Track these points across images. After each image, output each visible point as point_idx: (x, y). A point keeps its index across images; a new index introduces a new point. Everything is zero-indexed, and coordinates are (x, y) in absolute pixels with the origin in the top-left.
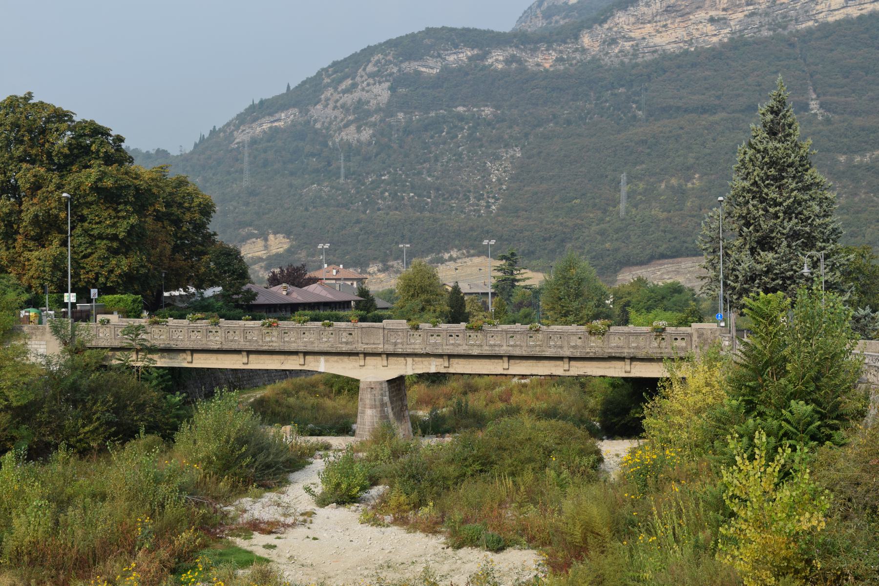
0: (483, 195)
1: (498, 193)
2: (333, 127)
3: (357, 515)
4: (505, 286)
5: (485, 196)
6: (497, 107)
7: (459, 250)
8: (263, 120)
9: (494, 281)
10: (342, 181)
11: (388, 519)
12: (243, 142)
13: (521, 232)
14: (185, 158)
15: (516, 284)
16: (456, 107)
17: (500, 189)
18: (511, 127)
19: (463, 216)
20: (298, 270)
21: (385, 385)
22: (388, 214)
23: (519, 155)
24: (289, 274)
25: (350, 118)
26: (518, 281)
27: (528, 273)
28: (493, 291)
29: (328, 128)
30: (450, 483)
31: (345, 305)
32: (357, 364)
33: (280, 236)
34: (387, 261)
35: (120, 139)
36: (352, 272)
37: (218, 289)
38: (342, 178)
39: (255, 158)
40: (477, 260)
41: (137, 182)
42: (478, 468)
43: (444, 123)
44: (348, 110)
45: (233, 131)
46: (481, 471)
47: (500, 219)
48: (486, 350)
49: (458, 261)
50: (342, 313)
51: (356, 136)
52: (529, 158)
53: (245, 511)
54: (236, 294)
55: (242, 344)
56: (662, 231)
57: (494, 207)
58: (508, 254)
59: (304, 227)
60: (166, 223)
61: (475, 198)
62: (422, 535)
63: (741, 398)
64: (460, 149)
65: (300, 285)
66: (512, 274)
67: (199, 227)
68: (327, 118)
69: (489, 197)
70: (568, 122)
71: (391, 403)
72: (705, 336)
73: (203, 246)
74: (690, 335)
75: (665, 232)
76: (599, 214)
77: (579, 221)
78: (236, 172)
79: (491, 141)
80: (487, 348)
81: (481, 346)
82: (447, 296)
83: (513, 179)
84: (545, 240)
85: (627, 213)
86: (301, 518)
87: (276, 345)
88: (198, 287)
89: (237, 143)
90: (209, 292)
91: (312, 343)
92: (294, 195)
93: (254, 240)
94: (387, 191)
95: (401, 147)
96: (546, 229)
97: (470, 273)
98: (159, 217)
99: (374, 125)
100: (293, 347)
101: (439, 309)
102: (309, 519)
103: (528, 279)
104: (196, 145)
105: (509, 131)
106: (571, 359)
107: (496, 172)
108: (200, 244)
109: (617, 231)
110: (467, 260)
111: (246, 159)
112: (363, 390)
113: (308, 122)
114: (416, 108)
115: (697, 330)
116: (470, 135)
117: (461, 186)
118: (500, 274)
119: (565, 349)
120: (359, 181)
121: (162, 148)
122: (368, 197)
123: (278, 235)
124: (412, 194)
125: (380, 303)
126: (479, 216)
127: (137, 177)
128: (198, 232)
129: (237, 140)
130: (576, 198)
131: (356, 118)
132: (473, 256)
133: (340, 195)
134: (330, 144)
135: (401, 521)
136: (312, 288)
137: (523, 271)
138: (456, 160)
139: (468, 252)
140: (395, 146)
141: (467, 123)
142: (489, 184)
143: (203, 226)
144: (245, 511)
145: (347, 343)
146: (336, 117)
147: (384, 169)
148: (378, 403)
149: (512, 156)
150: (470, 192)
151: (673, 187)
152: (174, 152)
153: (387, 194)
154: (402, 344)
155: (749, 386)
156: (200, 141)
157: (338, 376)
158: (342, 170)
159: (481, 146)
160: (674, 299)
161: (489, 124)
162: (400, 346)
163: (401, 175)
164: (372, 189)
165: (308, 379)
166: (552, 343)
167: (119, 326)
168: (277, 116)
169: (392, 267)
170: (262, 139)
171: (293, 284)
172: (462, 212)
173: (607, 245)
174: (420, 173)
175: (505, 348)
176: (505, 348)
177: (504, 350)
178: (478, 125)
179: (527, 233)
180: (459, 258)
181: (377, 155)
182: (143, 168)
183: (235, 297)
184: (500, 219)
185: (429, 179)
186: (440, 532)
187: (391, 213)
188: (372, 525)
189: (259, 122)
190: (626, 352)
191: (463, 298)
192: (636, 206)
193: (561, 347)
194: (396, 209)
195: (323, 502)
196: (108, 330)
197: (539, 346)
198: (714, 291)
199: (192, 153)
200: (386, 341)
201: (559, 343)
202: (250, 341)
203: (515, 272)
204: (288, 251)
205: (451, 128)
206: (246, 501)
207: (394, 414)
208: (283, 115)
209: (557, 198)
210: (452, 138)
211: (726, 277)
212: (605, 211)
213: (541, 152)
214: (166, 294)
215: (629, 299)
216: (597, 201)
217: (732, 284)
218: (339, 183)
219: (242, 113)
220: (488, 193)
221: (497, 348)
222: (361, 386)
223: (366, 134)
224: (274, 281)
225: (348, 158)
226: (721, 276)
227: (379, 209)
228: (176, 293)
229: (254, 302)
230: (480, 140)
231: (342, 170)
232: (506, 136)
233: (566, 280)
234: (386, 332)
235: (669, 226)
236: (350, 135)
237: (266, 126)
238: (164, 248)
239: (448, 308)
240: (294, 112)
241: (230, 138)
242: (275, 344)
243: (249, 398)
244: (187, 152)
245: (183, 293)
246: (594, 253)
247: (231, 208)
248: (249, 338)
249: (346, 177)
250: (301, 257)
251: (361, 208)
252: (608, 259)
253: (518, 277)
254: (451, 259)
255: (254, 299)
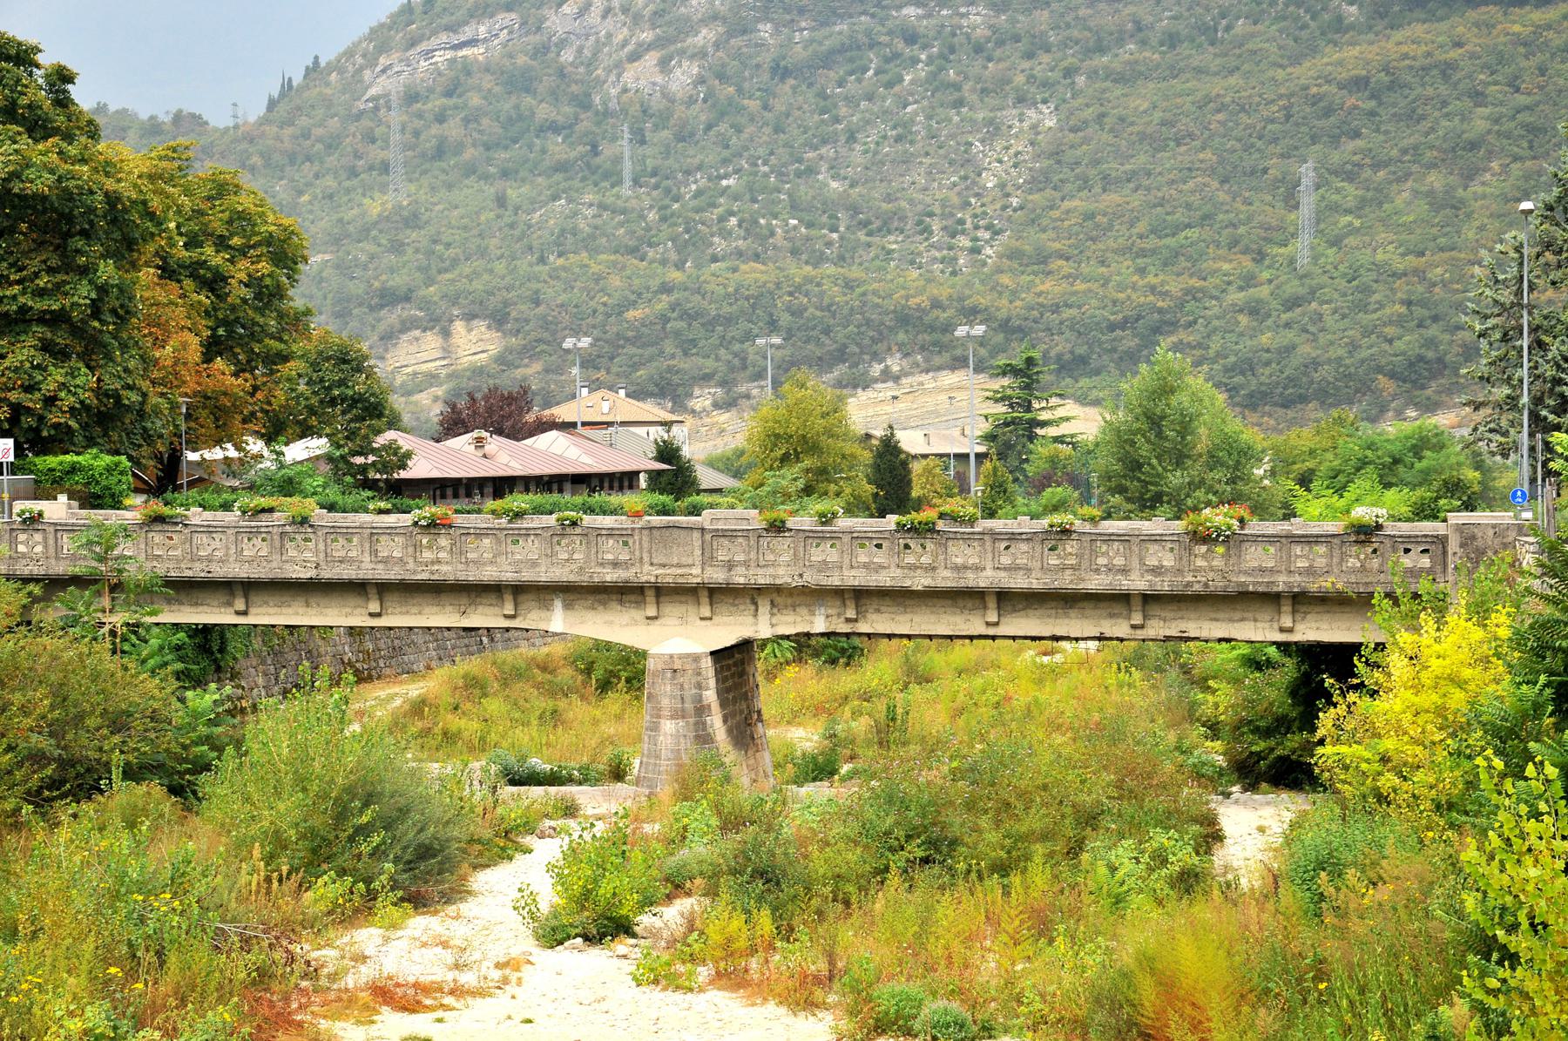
0: (962, 222)
1: (1000, 218)
2: (606, 60)
3: (628, 966)
4: (1012, 438)
5: (969, 225)
6: (998, 9)
7: (906, 355)
8: (434, 42)
9: (985, 427)
10: (626, 190)
11: (703, 973)
12: (387, 95)
13: (1056, 309)
14: (246, 136)
15: (1039, 431)
16: (899, 7)
17: (1004, 208)
18: (1030, 56)
19: (915, 274)
20: (510, 399)
21: (707, 663)
22: (735, 270)
23: (1050, 123)
24: (490, 410)
25: (646, 36)
26: (1043, 424)
27: (1070, 408)
28: (982, 449)
29: (590, 64)
30: (851, 888)
31: (624, 481)
32: (637, 614)
33: (481, 326)
34: (735, 382)
35: (63, 77)
36: (650, 410)
37: (316, 446)
38: (628, 183)
39: (417, 134)
40: (949, 378)
41: (110, 184)
42: (920, 853)
43: (871, 47)
44: (637, 19)
45: (361, 69)
46: (926, 861)
47: (1005, 279)
48: (945, 579)
49: (904, 381)
50: (615, 499)
51: (659, 79)
52: (1074, 130)
53: (362, 958)
54: (360, 454)
55: (368, 569)
56: (1402, 302)
57: (989, 251)
58: (1018, 362)
59: (537, 303)
60: (188, 283)
61: (944, 229)
62: (783, 1010)
63: (1543, 679)
64: (909, 109)
65: (518, 432)
66: (1029, 409)
67: (268, 295)
68: (587, 36)
69: (977, 228)
70: (1172, 40)
71: (723, 705)
72: (1479, 543)
73: (281, 340)
74: (1442, 541)
75: (1409, 303)
76: (1247, 263)
77: (1195, 282)
78: (371, 168)
79: (983, 90)
80: (947, 573)
81: (934, 569)
82: (866, 456)
83: (1038, 182)
84: (1112, 327)
85: (1315, 258)
86: (496, 975)
87: (448, 571)
88: (269, 439)
89: (373, 99)
90: (298, 451)
91: (534, 564)
92: (512, 226)
93: (417, 333)
94: (732, 214)
95: (765, 107)
96: (1114, 302)
97: (936, 414)
98: (168, 272)
99: (701, 54)
100: (488, 574)
101: (848, 491)
102: (514, 976)
103: (1068, 419)
104: (272, 104)
105: (1026, 65)
106: (1150, 600)
107: (996, 168)
108: (272, 337)
109: (1292, 303)
110: (924, 378)
111: (396, 137)
112: (655, 674)
113: (541, 51)
114: (802, 11)
115: (1460, 528)
116: (933, 76)
117: (911, 202)
118: (1001, 409)
119: (1135, 575)
120: (668, 191)
121: (189, 108)
122: (687, 231)
123: (475, 322)
124: (794, 222)
125: (707, 477)
126: (954, 273)
127: (108, 168)
128: (268, 305)
129: (373, 92)
130: (1189, 226)
131: (658, 38)
132: (939, 368)
133: (621, 224)
134: (597, 100)
135: (731, 978)
136: (550, 441)
137: (1054, 401)
138: (898, 139)
139: (927, 360)
140: (753, 105)
141: (924, 47)
142: (977, 195)
143: (278, 293)
144: (362, 958)
145: (615, 564)
146: (609, 36)
147: (725, 162)
148: (689, 706)
149: (1034, 127)
150: (931, 215)
151: (1431, 193)
152: (218, 118)
153: (733, 221)
154: (746, 564)
155: (1560, 649)
156: (282, 94)
157: (608, 646)
158: (627, 168)
159: (959, 103)
160: (1424, 464)
161: (978, 49)
162: (741, 570)
163: (766, 175)
164: (698, 210)
165: (525, 650)
166: (1102, 561)
167: (70, 529)
168: (467, 33)
169: (748, 397)
170: (431, 90)
171: (499, 432)
172: (912, 263)
173: (1265, 339)
174: (811, 171)
175: (989, 572)
176: (989, 572)
177: (987, 578)
178: (952, 50)
179: (1067, 313)
180: (906, 375)
181: (709, 127)
182: (131, 160)
183: (359, 460)
184: (1005, 279)
185: (834, 185)
186: (824, 1006)
187: (743, 267)
188: (665, 989)
189: (424, 46)
190: (1281, 583)
191: (904, 464)
192: (1336, 242)
193: (1124, 571)
194: (757, 257)
195: (554, 936)
196: (38, 537)
197: (1073, 568)
198: (1505, 434)
199: (263, 121)
200: (708, 559)
201: (1119, 561)
202: (385, 561)
203: (1036, 405)
204: (501, 359)
205: (887, 60)
206: (366, 937)
207: (730, 731)
208: (482, 29)
209: (1141, 227)
210: (889, 85)
211: (1538, 401)
212: (1260, 257)
213: (1103, 115)
214: (192, 456)
215: (1310, 464)
216: (1242, 230)
217: (1551, 417)
218: (618, 197)
219: (382, 25)
220: (975, 216)
221: (970, 575)
222: (651, 664)
223: (683, 76)
224: (453, 425)
225: (640, 139)
226: (1525, 399)
227: (715, 259)
228: (216, 454)
229: (403, 474)
230: (957, 87)
231: (627, 168)
232: (1020, 79)
233: (1155, 422)
234: (708, 537)
235: (1420, 289)
236: (642, 76)
237: (440, 57)
238: (185, 346)
239: (871, 489)
240: (507, 22)
241: (354, 85)
242: (444, 568)
243: (391, 698)
244: (252, 119)
245: (232, 453)
246: (1232, 359)
247: (363, 258)
248: (383, 554)
249: (636, 182)
250: (531, 372)
251: (673, 256)
252: (1267, 371)
253: (1044, 416)
254: (887, 376)
255: (404, 467)
